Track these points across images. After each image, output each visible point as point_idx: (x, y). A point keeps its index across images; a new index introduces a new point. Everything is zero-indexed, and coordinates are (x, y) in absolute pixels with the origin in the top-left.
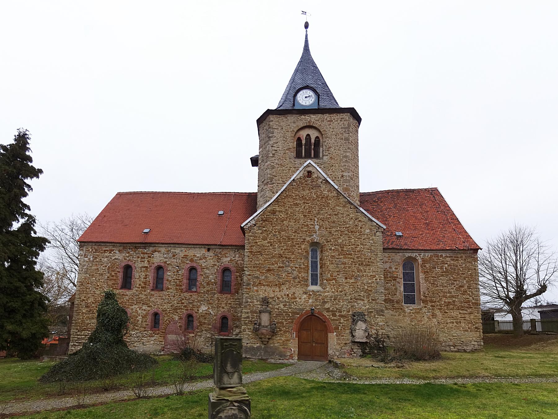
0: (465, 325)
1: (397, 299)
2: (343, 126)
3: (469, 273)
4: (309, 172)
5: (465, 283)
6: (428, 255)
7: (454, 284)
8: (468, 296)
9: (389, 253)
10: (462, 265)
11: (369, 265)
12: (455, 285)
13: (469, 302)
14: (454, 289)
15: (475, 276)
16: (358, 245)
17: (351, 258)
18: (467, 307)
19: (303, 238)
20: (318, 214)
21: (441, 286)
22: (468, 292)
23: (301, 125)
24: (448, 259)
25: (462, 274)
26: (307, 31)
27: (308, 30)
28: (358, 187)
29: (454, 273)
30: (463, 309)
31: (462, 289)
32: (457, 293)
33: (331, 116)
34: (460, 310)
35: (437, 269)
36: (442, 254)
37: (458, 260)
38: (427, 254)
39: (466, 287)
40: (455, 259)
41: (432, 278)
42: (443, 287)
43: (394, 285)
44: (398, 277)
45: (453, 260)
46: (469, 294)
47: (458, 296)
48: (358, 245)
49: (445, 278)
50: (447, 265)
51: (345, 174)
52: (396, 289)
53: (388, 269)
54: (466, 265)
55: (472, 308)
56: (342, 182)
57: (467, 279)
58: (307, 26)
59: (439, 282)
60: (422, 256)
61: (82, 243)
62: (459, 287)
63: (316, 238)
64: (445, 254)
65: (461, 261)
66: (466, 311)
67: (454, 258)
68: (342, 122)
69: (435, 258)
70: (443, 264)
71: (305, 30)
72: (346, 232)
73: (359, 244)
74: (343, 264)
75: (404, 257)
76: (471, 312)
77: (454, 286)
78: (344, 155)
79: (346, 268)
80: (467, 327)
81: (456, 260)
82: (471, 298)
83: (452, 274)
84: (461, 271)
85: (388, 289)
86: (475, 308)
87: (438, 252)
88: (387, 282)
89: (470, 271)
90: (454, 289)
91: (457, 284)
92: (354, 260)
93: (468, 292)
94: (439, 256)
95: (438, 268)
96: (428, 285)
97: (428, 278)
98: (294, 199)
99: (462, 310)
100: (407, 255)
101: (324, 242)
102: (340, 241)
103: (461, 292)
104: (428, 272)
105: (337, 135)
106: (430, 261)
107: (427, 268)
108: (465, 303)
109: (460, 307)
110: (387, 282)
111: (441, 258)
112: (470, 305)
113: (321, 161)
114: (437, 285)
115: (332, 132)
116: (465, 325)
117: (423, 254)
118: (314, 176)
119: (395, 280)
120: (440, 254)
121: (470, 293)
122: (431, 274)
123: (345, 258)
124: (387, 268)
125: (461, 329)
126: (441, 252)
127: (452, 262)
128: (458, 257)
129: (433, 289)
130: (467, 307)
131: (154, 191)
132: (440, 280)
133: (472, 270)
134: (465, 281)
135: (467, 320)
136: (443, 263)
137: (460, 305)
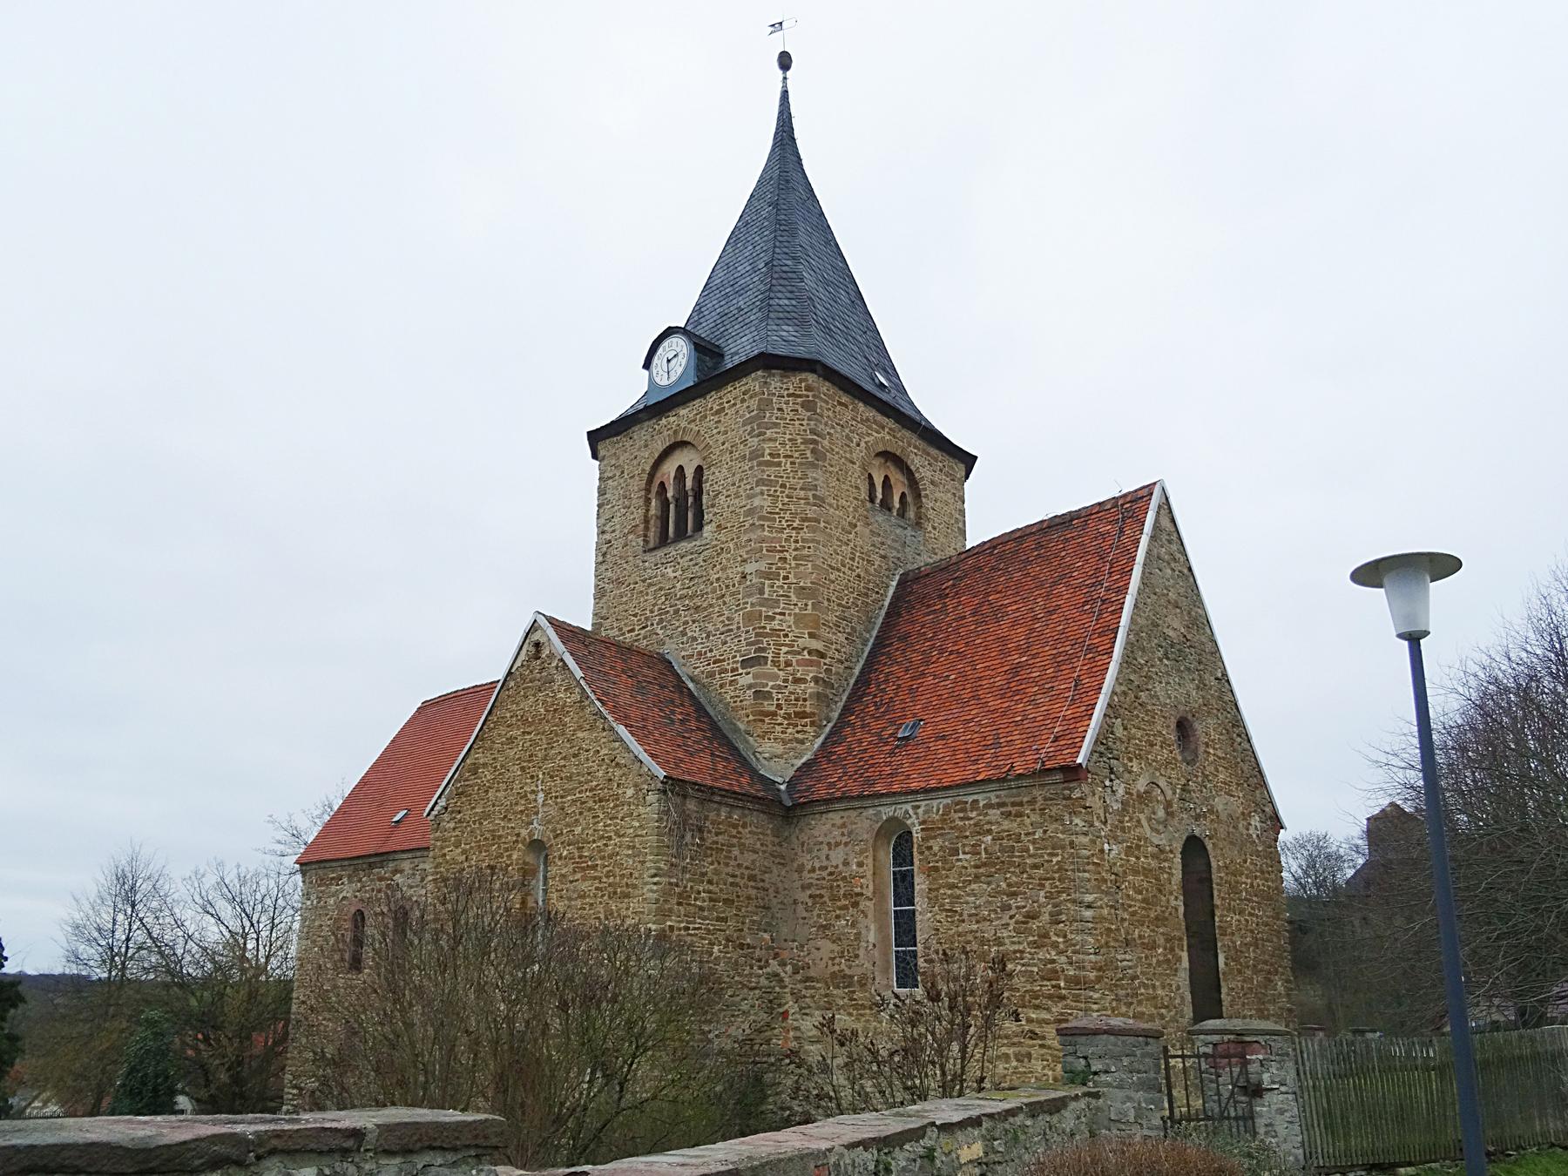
0: (1044, 1068)
1: (859, 971)
2: (748, 416)
3: (1055, 860)
4: (537, 645)
5: (1042, 900)
6: (938, 804)
7: (1008, 907)
8: (1053, 953)
9: (842, 813)
10: (1034, 833)
11: (627, 896)
12: (1012, 912)
13: (1054, 975)
14: (1011, 928)
15: (1073, 870)
16: (610, 838)
17: (595, 878)
18: (1050, 997)
19: (516, 831)
20: (545, 758)
21: (973, 919)
22: (1054, 938)
23: (659, 446)
24: (994, 814)
25: (1035, 866)
26: (785, 78)
27: (789, 74)
28: (963, 532)
29: (1012, 864)
30: (1037, 1002)
31: (1034, 925)
32: (1019, 943)
33: (722, 393)
34: (1030, 1007)
35: (961, 856)
36: (975, 797)
37: (1019, 815)
38: (935, 803)
39: (1046, 917)
40: (1014, 810)
41: (949, 892)
42: (978, 922)
43: (853, 925)
44: (862, 894)
45: (1008, 815)
46: (1055, 945)
47: (1022, 952)
48: (610, 838)
49: (985, 886)
50: (990, 838)
51: (750, 568)
52: (858, 936)
53: (841, 866)
54: (1045, 832)
55: (1063, 998)
56: (740, 596)
57: (1047, 883)
58: (785, 61)
59: (967, 903)
60: (920, 811)
61: (305, 865)
62: (1024, 917)
63: (538, 829)
64: (985, 795)
65: (1032, 816)
66: (1048, 1010)
67: (1010, 808)
68: (745, 405)
69: (957, 816)
70: (979, 833)
71: (780, 73)
72: (591, 804)
73: (612, 834)
74: (580, 897)
75: (877, 822)
76: (1062, 1014)
77: (1011, 917)
78: (748, 507)
79: (585, 909)
80: (1050, 1073)
81: (1016, 816)
82: (1063, 959)
83: (1004, 867)
84: (1030, 856)
85: (840, 939)
86: (1077, 999)
87: (962, 791)
88: (838, 912)
89: (1057, 855)
90: (1011, 928)
91: (1018, 908)
92: (600, 882)
93: (1054, 938)
94: (968, 806)
95: (964, 853)
96: (938, 917)
97: (937, 890)
98: (508, 726)
99: (1037, 1007)
100: (887, 812)
101: (549, 839)
102: (578, 830)
103: (1031, 938)
104: (936, 869)
105: (734, 449)
106: (942, 828)
107: (935, 855)
108: (1043, 978)
109: (1027, 997)
110: (838, 912)
111: (973, 814)
112: (1060, 988)
113: (698, 543)
114: (961, 915)
115: (723, 444)
116: (1044, 1068)
117: (923, 803)
118: (545, 653)
119: (855, 905)
120: (970, 799)
121: (1061, 940)
122: (947, 877)
123: (584, 879)
124: (837, 867)
125: (1033, 1080)
126: (970, 790)
127: (1006, 824)
128: (1021, 804)
129: (951, 932)
130: (1050, 997)
131: (466, 687)
132: (968, 895)
133: (1063, 848)
134: (1042, 893)
135: (1049, 1048)
136: (980, 831)
137: (1029, 987)
